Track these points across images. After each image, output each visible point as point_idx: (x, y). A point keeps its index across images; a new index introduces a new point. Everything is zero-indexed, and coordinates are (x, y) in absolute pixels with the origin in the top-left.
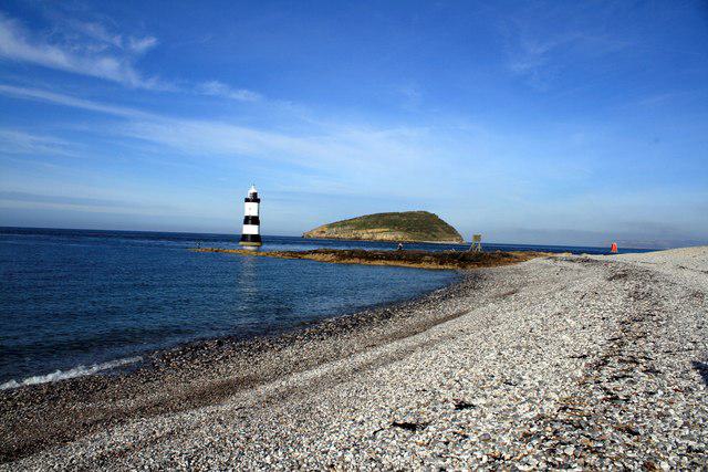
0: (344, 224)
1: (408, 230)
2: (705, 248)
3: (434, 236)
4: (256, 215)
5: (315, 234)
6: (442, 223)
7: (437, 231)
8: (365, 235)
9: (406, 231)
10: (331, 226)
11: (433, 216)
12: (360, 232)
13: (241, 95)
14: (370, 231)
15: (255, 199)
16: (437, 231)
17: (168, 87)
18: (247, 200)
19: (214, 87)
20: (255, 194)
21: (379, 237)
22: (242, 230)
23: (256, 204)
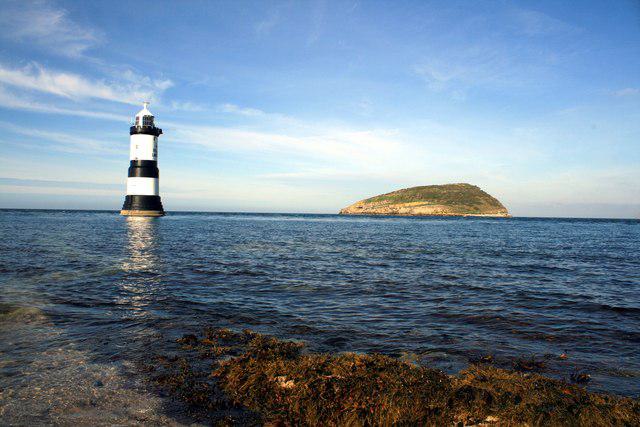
0: (381, 198)
1: (449, 203)
2: (638, 225)
3: (477, 209)
4: (151, 158)
5: (353, 210)
6: (484, 194)
7: (480, 204)
8: (402, 209)
9: (445, 204)
10: (368, 201)
11: (466, 185)
12: (398, 206)
13: (248, 112)
14: (407, 205)
15: (151, 129)
16: (480, 204)
17: (198, 108)
18: (134, 131)
19: (229, 108)
20: (148, 120)
21: (417, 211)
22: (124, 187)
23: (150, 138)
